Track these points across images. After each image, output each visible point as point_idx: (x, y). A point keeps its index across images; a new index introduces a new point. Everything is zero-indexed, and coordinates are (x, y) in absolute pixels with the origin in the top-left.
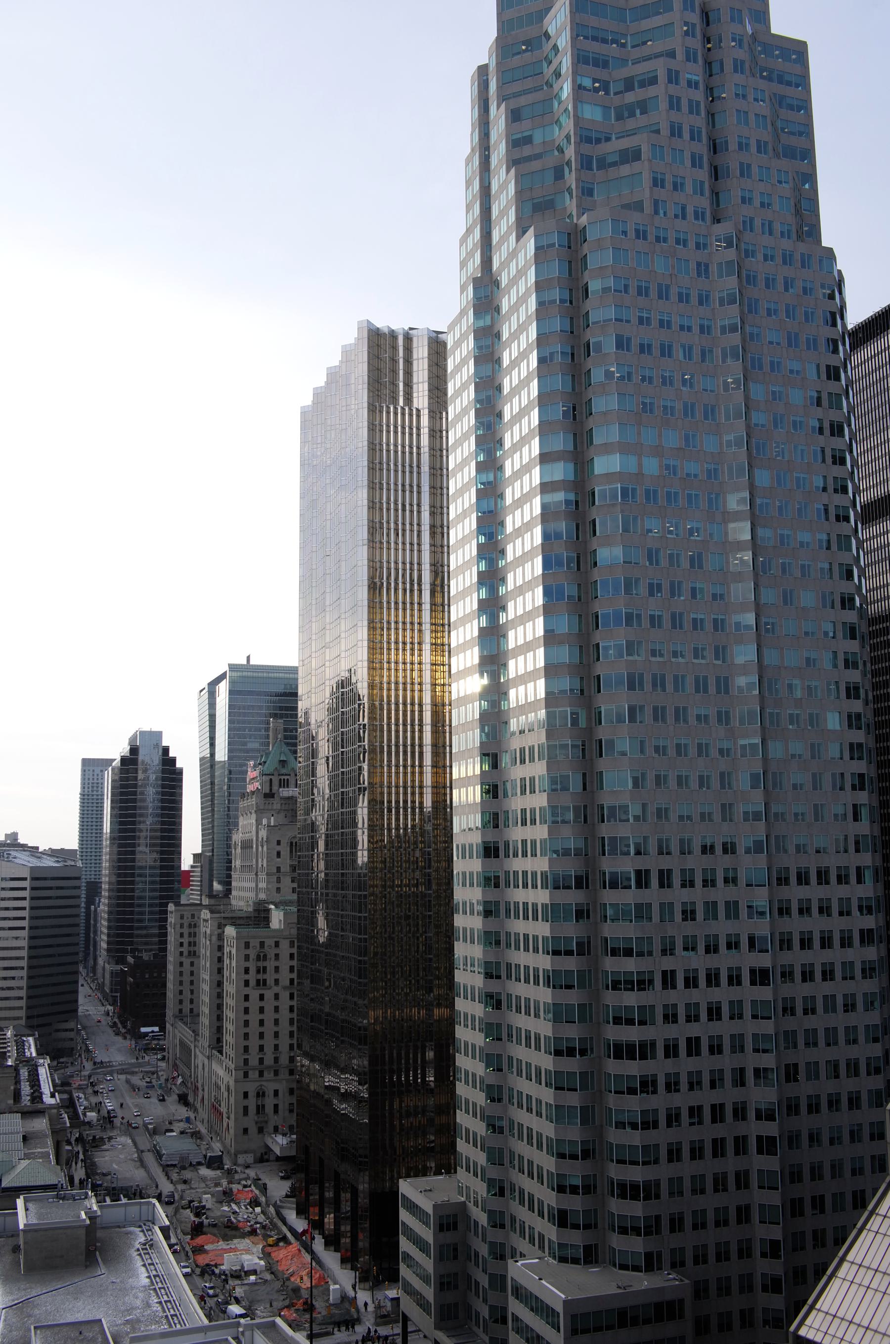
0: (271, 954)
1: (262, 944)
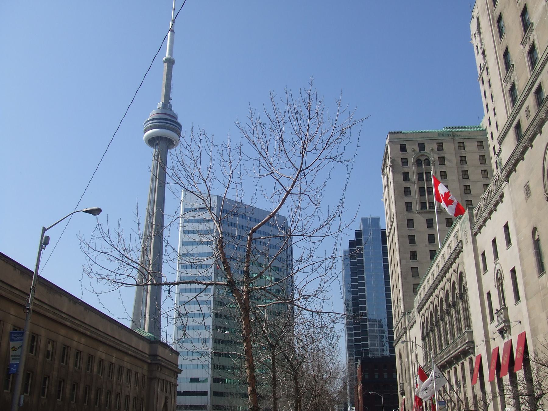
0: (434, 158)
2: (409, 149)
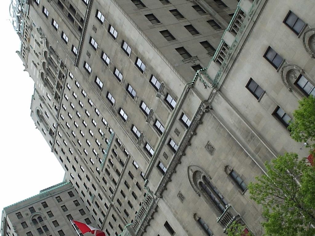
1: (32, 210)
2: (23, 215)
